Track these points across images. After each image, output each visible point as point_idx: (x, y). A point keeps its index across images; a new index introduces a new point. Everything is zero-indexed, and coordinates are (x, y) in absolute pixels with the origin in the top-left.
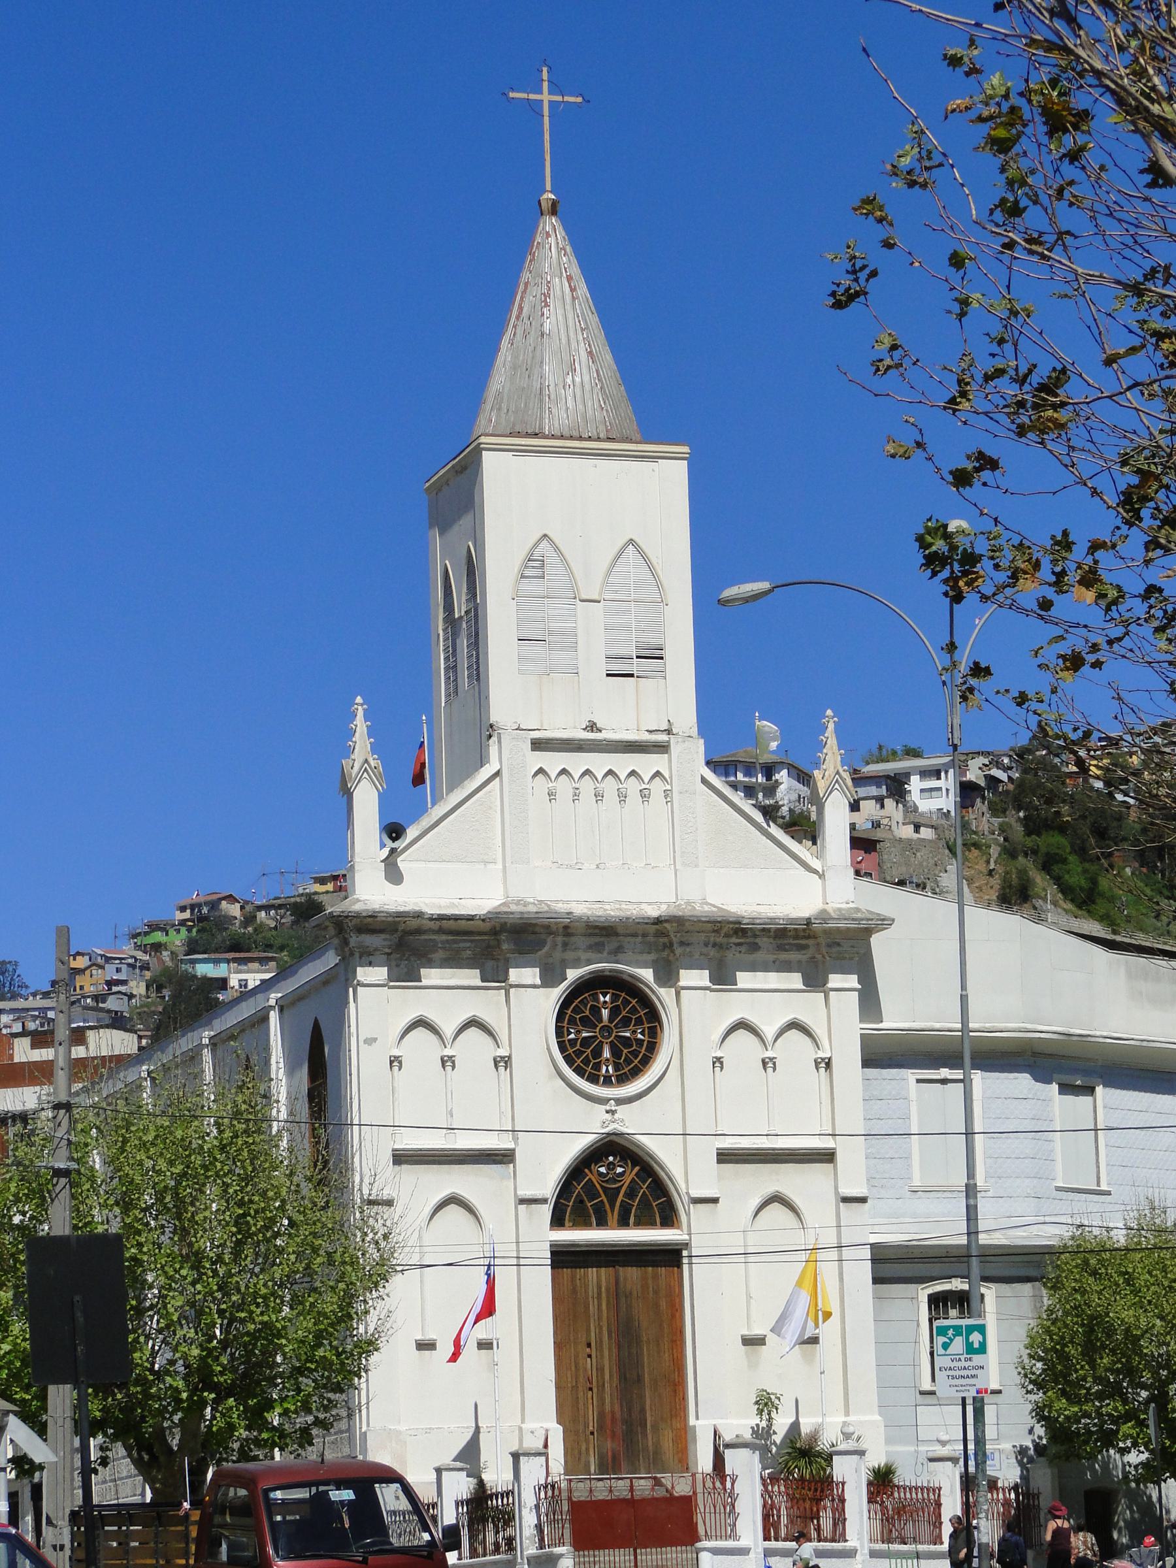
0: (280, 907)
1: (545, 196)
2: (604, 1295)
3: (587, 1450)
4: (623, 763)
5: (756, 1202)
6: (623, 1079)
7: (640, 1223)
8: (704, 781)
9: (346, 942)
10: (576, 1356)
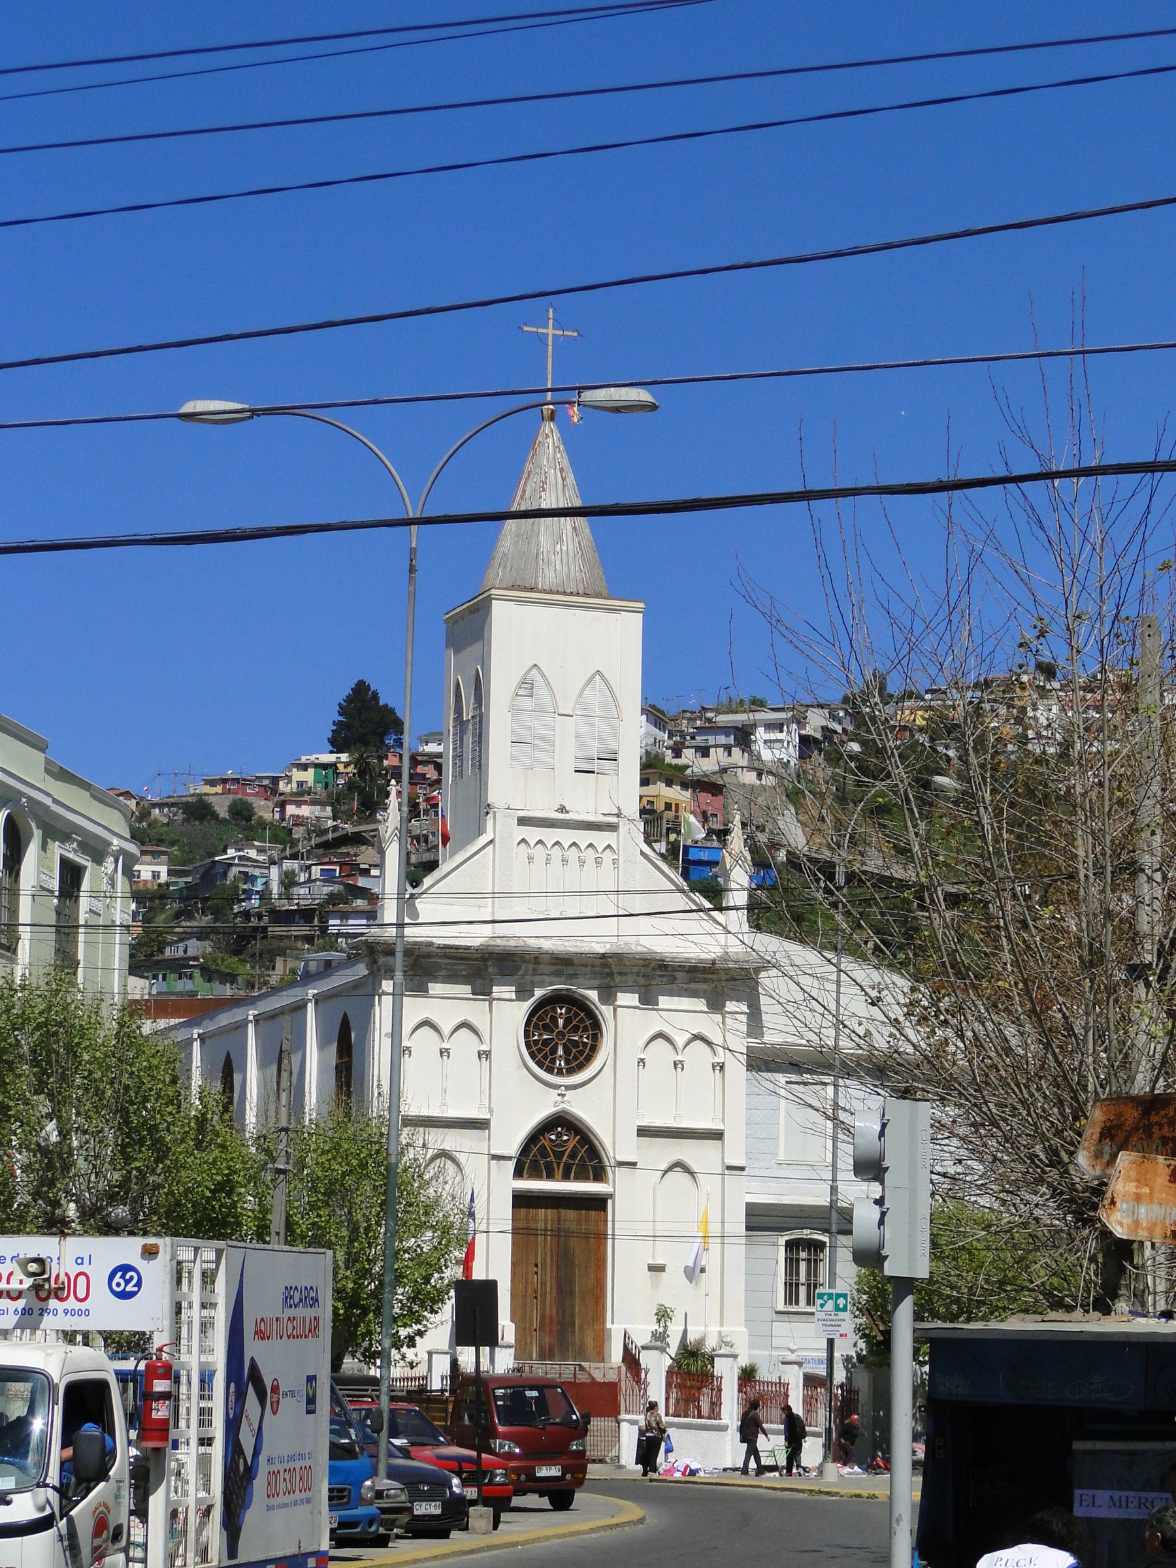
0: (173, 805)
4: (584, 837)
5: (664, 1166)
6: (571, 1071)
8: (642, 853)
9: (376, 962)
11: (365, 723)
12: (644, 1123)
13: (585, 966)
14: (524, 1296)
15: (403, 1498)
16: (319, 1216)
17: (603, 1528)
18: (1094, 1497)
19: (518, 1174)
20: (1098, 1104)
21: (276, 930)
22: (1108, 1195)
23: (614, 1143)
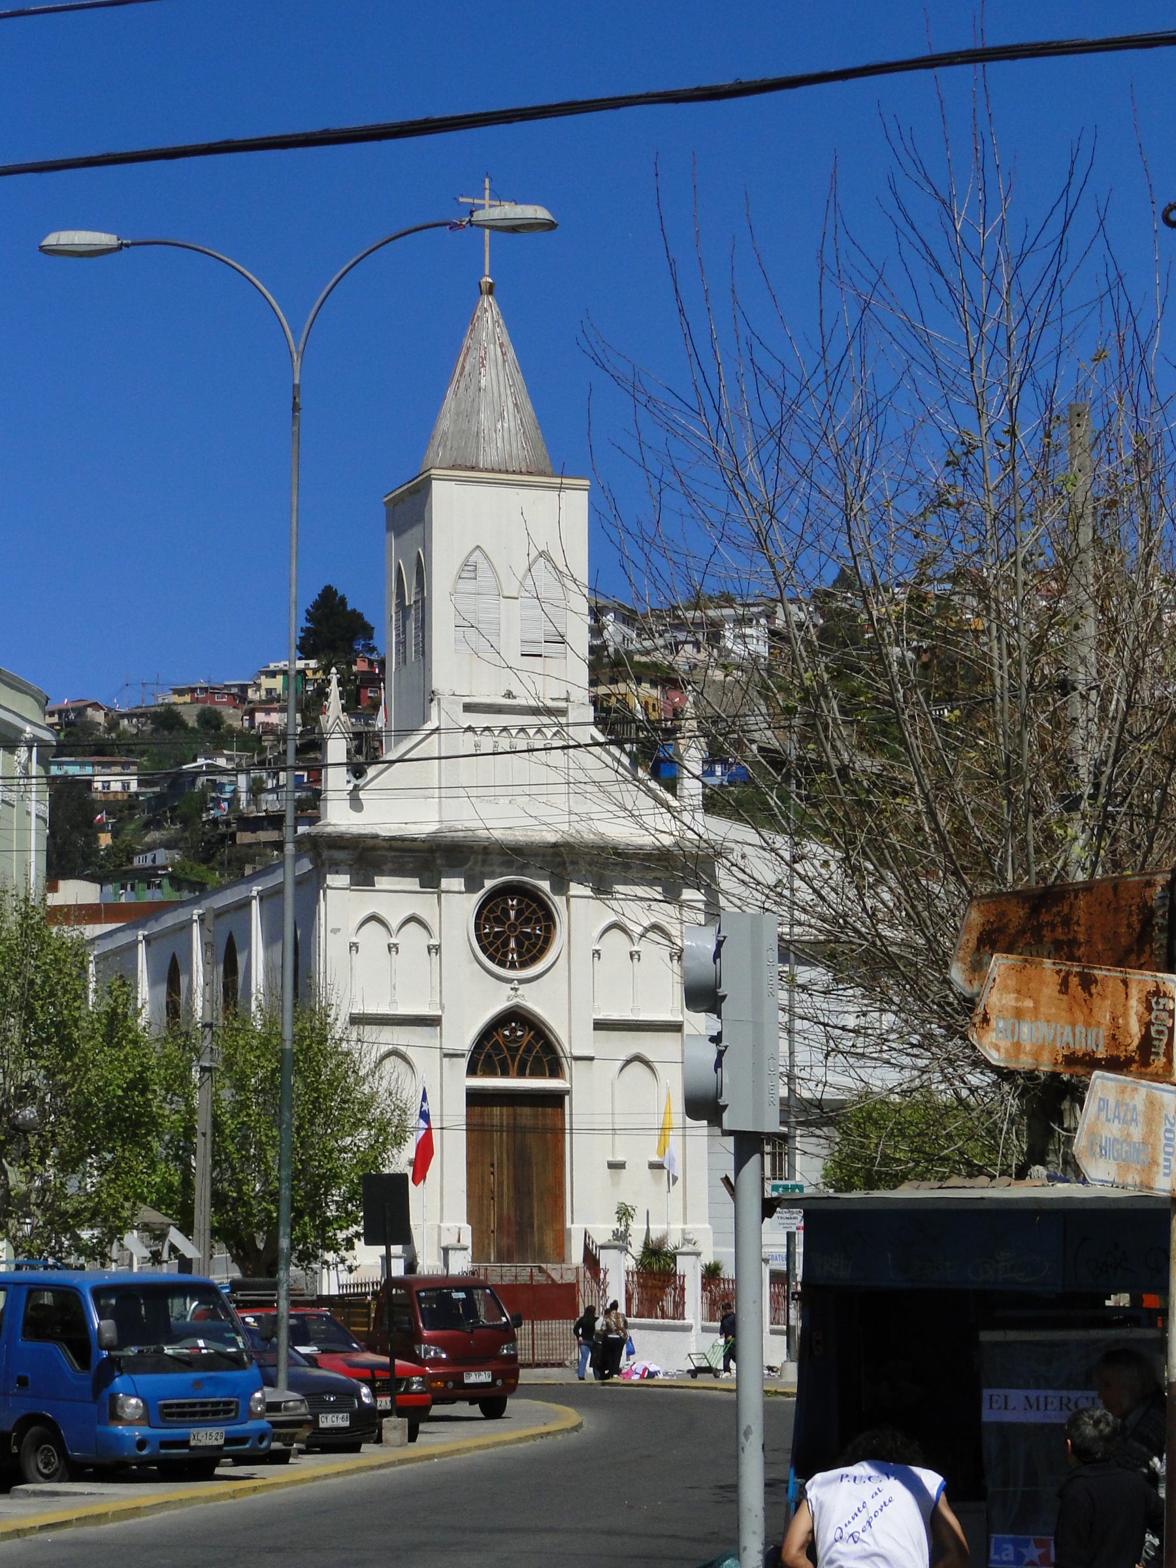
0: (142, 715)
1: (484, 280)
3: (489, 1244)
6: (524, 965)
9: (319, 855)
11: (335, 631)
12: (600, 1016)
13: (536, 855)
14: (481, 1197)
15: (303, 1410)
16: (249, 1115)
17: (533, 1437)
18: (1006, 1397)
19: (472, 1071)
20: (975, 903)
21: (244, 838)
22: (980, 1010)
23: (570, 1037)
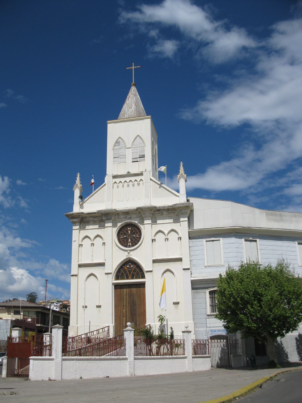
2: (127, 294)
6: (133, 246)
7: (136, 278)
10: (121, 309)
19: (117, 278)
